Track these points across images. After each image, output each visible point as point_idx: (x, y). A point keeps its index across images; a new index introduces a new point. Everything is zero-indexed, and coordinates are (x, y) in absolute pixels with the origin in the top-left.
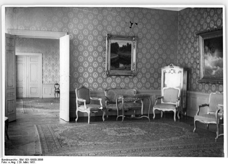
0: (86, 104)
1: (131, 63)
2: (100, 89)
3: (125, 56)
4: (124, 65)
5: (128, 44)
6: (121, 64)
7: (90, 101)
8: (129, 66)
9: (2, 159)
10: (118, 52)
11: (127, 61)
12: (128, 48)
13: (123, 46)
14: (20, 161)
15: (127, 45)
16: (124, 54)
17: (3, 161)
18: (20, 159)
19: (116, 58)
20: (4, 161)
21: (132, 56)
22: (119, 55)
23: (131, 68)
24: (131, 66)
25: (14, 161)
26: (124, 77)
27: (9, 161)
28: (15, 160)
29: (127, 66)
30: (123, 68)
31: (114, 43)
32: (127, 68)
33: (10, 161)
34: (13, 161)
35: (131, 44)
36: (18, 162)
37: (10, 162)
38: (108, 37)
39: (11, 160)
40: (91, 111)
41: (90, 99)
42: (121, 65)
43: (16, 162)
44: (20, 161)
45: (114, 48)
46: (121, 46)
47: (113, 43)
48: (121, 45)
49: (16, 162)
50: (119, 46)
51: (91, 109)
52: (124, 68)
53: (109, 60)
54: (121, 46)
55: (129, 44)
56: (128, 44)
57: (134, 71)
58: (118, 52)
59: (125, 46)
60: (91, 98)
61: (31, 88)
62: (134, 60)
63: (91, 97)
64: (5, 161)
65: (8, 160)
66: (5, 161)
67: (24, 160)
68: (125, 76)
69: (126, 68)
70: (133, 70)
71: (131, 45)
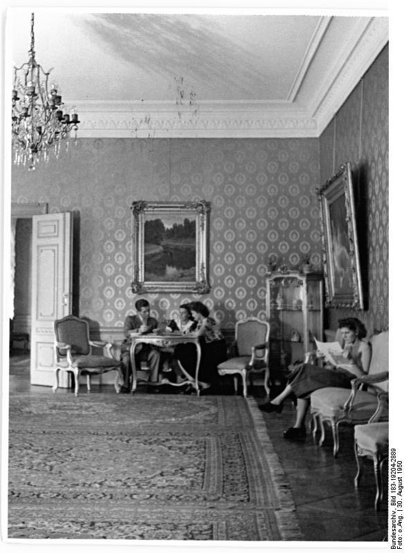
0: (73, 355)
1: (195, 265)
2: (120, 324)
3: (180, 248)
4: (178, 268)
5: (186, 221)
6: (169, 266)
7: (89, 349)
8: (192, 272)
9: (393, 548)
10: (162, 240)
11: (186, 260)
12: (188, 230)
13: (175, 226)
14: (397, 504)
15: (183, 225)
16: (177, 244)
17: (396, 546)
18: (393, 504)
19: (159, 254)
20: (397, 543)
21: (197, 249)
22: (165, 247)
23: (195, 274)
24: (195, 272)
25: (397, 520)
26: (179, 295)
27: (397, 532)
28: (394, 516)
29: (186, 272)
30: (175, 276)
31: (151, 221)
32: (186, 276)
33: (398, 528)
34: (397, 522)
35: (195, 222)
36: (399, 508)
37: (400, 528)
38: (135, 208)
39: (394, 526)
40: (79, 368)
41: (89, 345)
42: (171, 270)
43: (398, 514)
44: (397, 504)
45: (153, 231)
46: (168, 226)
47: (149, 220)
48: (169, 225)
49: (398, 514)
50: (164, 228)
51: (79, 364)
52: (180, 275)
53: (143, 257)
54: (168, 226)
55: (191, 220)
56: (186, 221)
57: (202, 282)
58: (162, 240)
59: (181, 226)
60: (91, 343)
61: (57, 236)
62: (201, 257)
63: (92, 340)
64: (397, 540)
65: (394, 534)
66: (397, 540)
67: (394, 494)
68: (183, 293)
69: (182, 276)
70: (201, 280)
71: (194, 223)
